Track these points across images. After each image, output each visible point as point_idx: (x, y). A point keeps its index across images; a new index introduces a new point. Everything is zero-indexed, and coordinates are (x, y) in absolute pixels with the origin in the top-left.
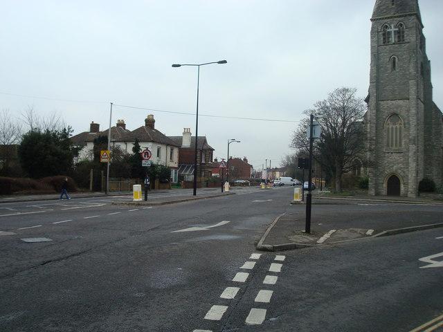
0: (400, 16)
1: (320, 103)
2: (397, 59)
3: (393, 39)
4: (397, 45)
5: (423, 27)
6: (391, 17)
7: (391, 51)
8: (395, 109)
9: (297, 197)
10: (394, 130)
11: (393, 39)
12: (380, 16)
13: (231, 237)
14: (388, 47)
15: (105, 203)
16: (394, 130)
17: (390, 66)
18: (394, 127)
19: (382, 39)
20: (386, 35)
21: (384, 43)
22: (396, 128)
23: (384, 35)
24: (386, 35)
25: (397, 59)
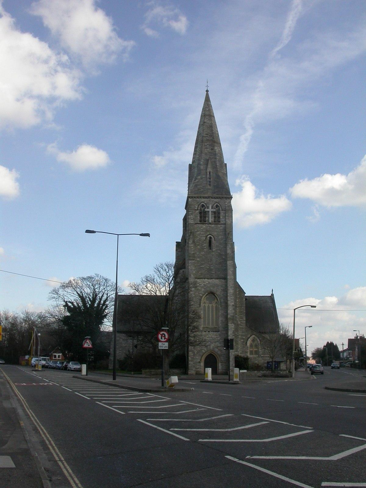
0: (217, 198)
1: (27, 313)
2: (213, 238)
3: (211, 219)
4: (213, 226)
5: (178, 243)
6: (209, 197)
7: (207, 231)
8: (212, 288)
9: (236, 377)
10: (211, 308)
11: (211, 219)
12: (195, 194)
13: (114, 406)
14: (204, 226)
15: (267, 421)
16: (211, 308)
17: (206, 245)
18: (210, 305)
19: (199, 218)
20: (203, 215)
21: (200, 221)
22: (212, 307)
23: (200, 213)
24: (203, 215)
25: (213, 238)
